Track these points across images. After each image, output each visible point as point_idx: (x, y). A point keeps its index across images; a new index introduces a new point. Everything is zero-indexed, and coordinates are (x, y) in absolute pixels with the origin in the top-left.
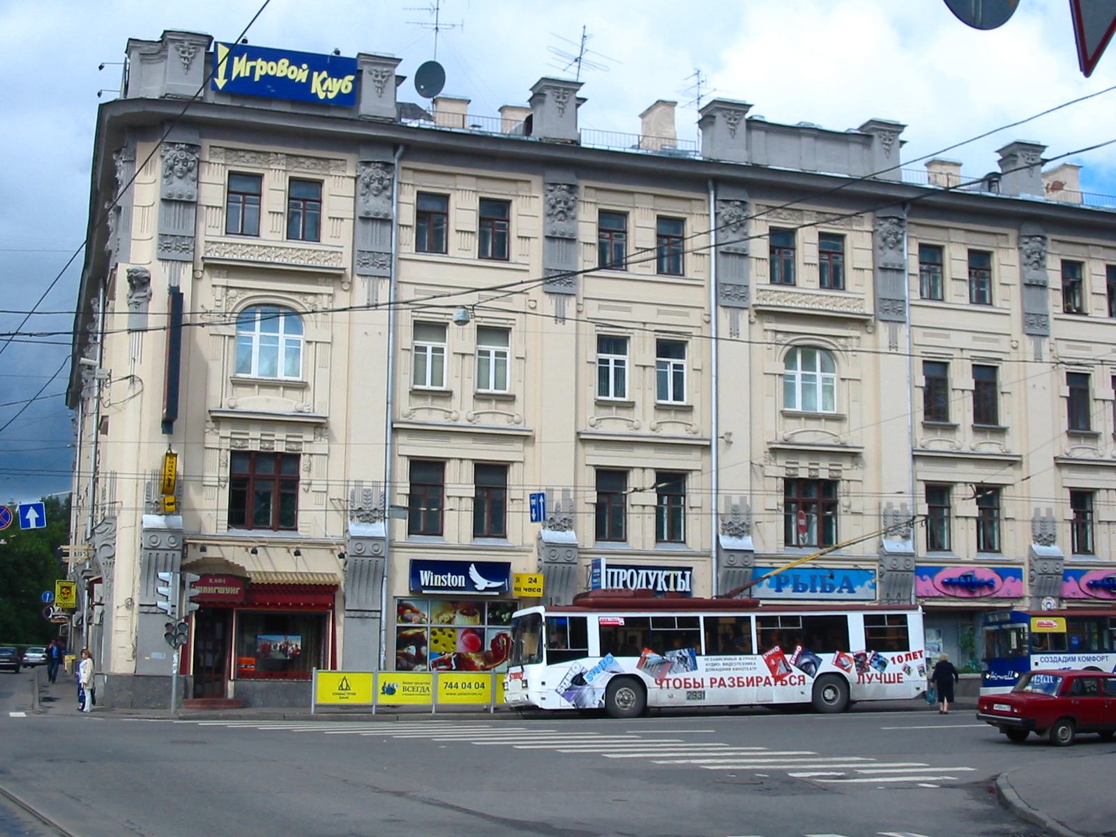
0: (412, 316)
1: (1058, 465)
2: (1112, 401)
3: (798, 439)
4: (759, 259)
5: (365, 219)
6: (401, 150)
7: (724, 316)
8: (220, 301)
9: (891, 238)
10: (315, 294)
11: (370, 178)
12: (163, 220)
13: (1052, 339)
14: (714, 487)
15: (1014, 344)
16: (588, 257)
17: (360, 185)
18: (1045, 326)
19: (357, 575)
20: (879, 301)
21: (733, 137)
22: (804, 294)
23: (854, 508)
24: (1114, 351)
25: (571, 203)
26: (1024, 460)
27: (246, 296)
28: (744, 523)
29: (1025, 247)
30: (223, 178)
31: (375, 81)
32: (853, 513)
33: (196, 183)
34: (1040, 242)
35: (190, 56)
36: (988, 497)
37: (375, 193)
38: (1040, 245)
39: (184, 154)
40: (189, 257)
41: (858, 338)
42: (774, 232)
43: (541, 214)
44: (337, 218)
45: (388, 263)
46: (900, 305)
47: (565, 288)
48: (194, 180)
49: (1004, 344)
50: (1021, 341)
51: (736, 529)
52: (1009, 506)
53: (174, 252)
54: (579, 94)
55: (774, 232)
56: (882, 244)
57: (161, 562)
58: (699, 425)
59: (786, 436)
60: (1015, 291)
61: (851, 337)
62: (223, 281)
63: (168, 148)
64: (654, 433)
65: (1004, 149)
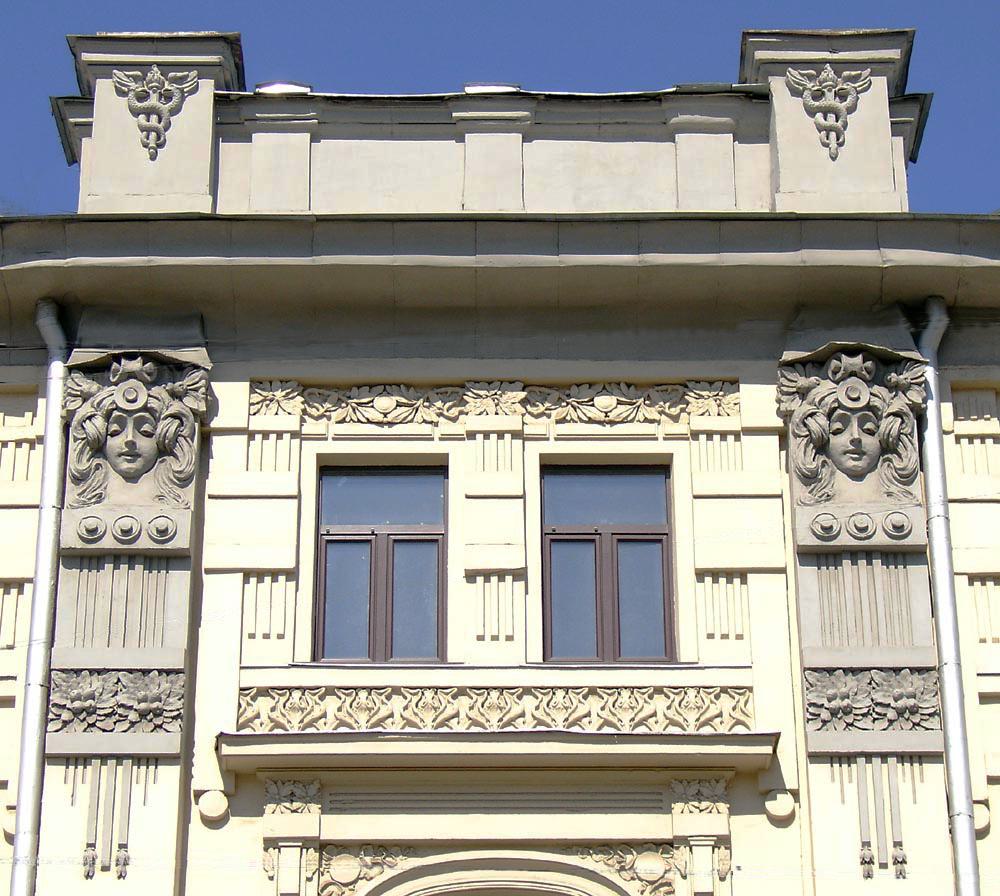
4: (260, 574)
10: (664, 846)
11: (108, 416)
21: (153, 157)
27: (389, 873)
30: (520, 470)
31: (135, 113)
40: (168, 741)
41: (722, 842)
45: (176, 704)
47: (139, 735)
61: (684, 841)
62: (309, 821)
63: (802, 382)
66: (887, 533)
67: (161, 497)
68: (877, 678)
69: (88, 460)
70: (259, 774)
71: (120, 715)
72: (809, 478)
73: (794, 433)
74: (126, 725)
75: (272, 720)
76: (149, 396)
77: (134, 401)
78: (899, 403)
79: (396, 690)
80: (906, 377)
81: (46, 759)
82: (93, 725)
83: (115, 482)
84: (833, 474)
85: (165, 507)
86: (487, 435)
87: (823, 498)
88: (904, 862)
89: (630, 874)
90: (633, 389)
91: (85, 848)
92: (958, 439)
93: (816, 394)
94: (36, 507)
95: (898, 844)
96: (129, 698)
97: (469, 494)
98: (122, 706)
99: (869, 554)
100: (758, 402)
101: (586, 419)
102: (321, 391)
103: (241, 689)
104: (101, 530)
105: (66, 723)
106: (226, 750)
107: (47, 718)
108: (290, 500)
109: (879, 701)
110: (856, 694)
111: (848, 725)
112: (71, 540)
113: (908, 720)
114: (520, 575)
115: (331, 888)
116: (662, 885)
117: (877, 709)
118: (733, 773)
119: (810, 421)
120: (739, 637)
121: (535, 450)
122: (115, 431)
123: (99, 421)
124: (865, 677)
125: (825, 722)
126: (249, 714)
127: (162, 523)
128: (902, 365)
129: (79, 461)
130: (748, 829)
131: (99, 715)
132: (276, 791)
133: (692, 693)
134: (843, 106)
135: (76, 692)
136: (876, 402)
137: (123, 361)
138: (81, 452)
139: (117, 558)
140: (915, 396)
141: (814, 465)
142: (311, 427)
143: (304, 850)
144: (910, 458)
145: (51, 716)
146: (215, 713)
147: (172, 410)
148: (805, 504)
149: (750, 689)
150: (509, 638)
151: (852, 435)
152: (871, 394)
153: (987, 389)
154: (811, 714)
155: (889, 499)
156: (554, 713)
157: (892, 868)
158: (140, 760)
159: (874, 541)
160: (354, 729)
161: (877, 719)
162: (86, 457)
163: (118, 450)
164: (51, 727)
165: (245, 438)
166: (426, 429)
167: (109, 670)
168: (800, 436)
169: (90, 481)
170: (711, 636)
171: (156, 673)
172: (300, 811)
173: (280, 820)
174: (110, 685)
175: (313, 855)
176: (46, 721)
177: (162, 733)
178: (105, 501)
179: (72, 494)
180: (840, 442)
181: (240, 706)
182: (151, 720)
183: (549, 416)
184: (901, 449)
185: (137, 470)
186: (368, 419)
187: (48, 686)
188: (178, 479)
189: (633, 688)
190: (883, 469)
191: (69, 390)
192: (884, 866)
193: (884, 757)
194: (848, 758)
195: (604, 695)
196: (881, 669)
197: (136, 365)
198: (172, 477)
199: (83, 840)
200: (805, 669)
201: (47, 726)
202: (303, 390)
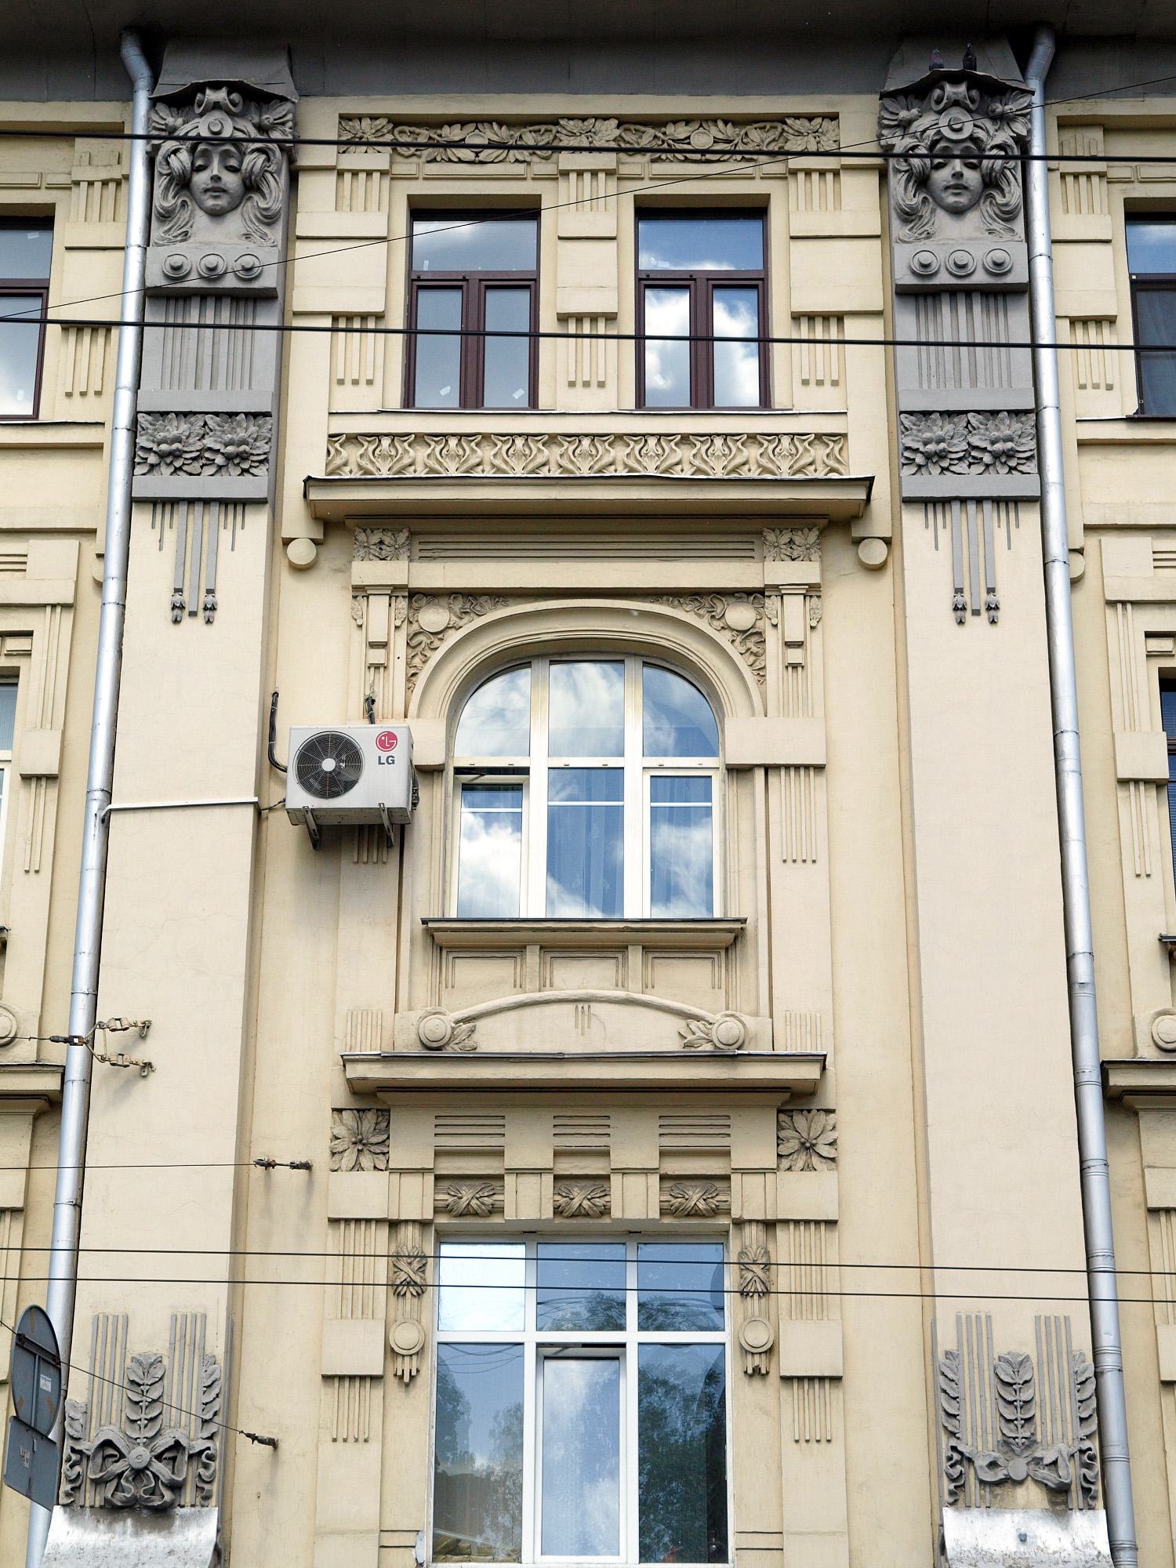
0: (1150, 655)
2: (1158, 784)
3: (493, 1037)
6: (1043, 51)
8: (384, 645)
10: (754, 595)
14: (1105, 1310)
23: (791, 1362)
24: (1161, 560)
28: (177, 1446)
32: (787, 1380)
33: (276, 233)
41: (812, 591)
47: (991, 476)
51: (138, 1473)
59: (438, 1027)
63: (904, 114)
66: (951, 273)
67: (247, 236)
68: (974, 422)
69: (174, 197)
70: (347, 521)
71: (207, 459)
73: (894, 168)
74: (145, 469)
75: (760, 466)
76: (235, 128)
77: (959, 130)
78: (1003, 136)
79: (486, 437)
80: (1011, 107)
81: (133, 501)
82: (180, 469)
83: (201, 220)
84: (933, 211)
85: (252, 245)
86: (580, 173)
87: (923, 236)
88: (997, 608)
89: (720, 624)
91: (953, 594)
92: (1063, 176)
93: (918, 126)
94: (122, 249)
95: (991, 591)
96: (216, 441)
97: (561, 235)
98: (210, 449)
101: (456, 160)
102: (412, 129)
103: (331, 436)
104: (186, 268)
105: (152, 467)
106: (315, 495)
107: (134, 462)
108: (304, 235)
109: (975, 444)
110: (952, 437)
111: (1011, 469)
112: (156, 280)
113: (1005, 463)
115: (420, 638)
116: (752, 634)
117: (973, 453)
118: (826, 521)
119: (173, 159)
120: (835, 383)
122: (200, 166)
123: (184, 156)
124: (963, 418)
125: (920, 467)
126: (338, 461)
127: (248, 261)
128: (1007, 95)
129: (165, 197)
131: (186, 459)
132: (774, 539)
133: (786, 441)
135: (162, 434)
136: (981, 134)
137: (208, 91)
138: (167, 189)
140: (1020, 128)
141: (915, 200)
143: (394, 598)
144: (1013, 194)
145: (137, 460)
147: (998, 141)
148: (905, 242)
149: (845, 436)
150: (601, 385)
151: (953, 169)
152: (235, 128)
153: (680, 121)
154: (907, 458)
155: (990, 236)
156: (513, 462)
157: (984, 614)
158: (1001, 502)
159: (936, 281)
160: (709, 475)
161: (973, 463)
162: (171, 194)
163: (204, 186)
164: (139, 470)
165: (333, 177)
166: (520, 169)
167: (195, 413)
168: (900, 172)
169: (175, 220)
170: (805, 382)
171: (243, 416)
172: (389, 558)
174: (197, 428)
175: (403, 604)
176: (133, 465)
177: (247, 476)
178: (191, 240)
179: (157, 232)
180: (942, 177)
181: (329, 452)
182: (238, 464)
183: (420, 157)
184: (1004, 186)
185: (222, 208)
186: (459, 159)
187: (134, 429)
188: (266, 217)
189: (794, 435)
190: (248, 208)
191: (154, 124)
192: (976, 613)
193: (979, 501)
194: (944, 502)
195: (697, 443)
196: (978, 412)
197: (221, 95)
198: (259, 216)
200: (901, 413)
201: (134, 469)
202: (394, 128)
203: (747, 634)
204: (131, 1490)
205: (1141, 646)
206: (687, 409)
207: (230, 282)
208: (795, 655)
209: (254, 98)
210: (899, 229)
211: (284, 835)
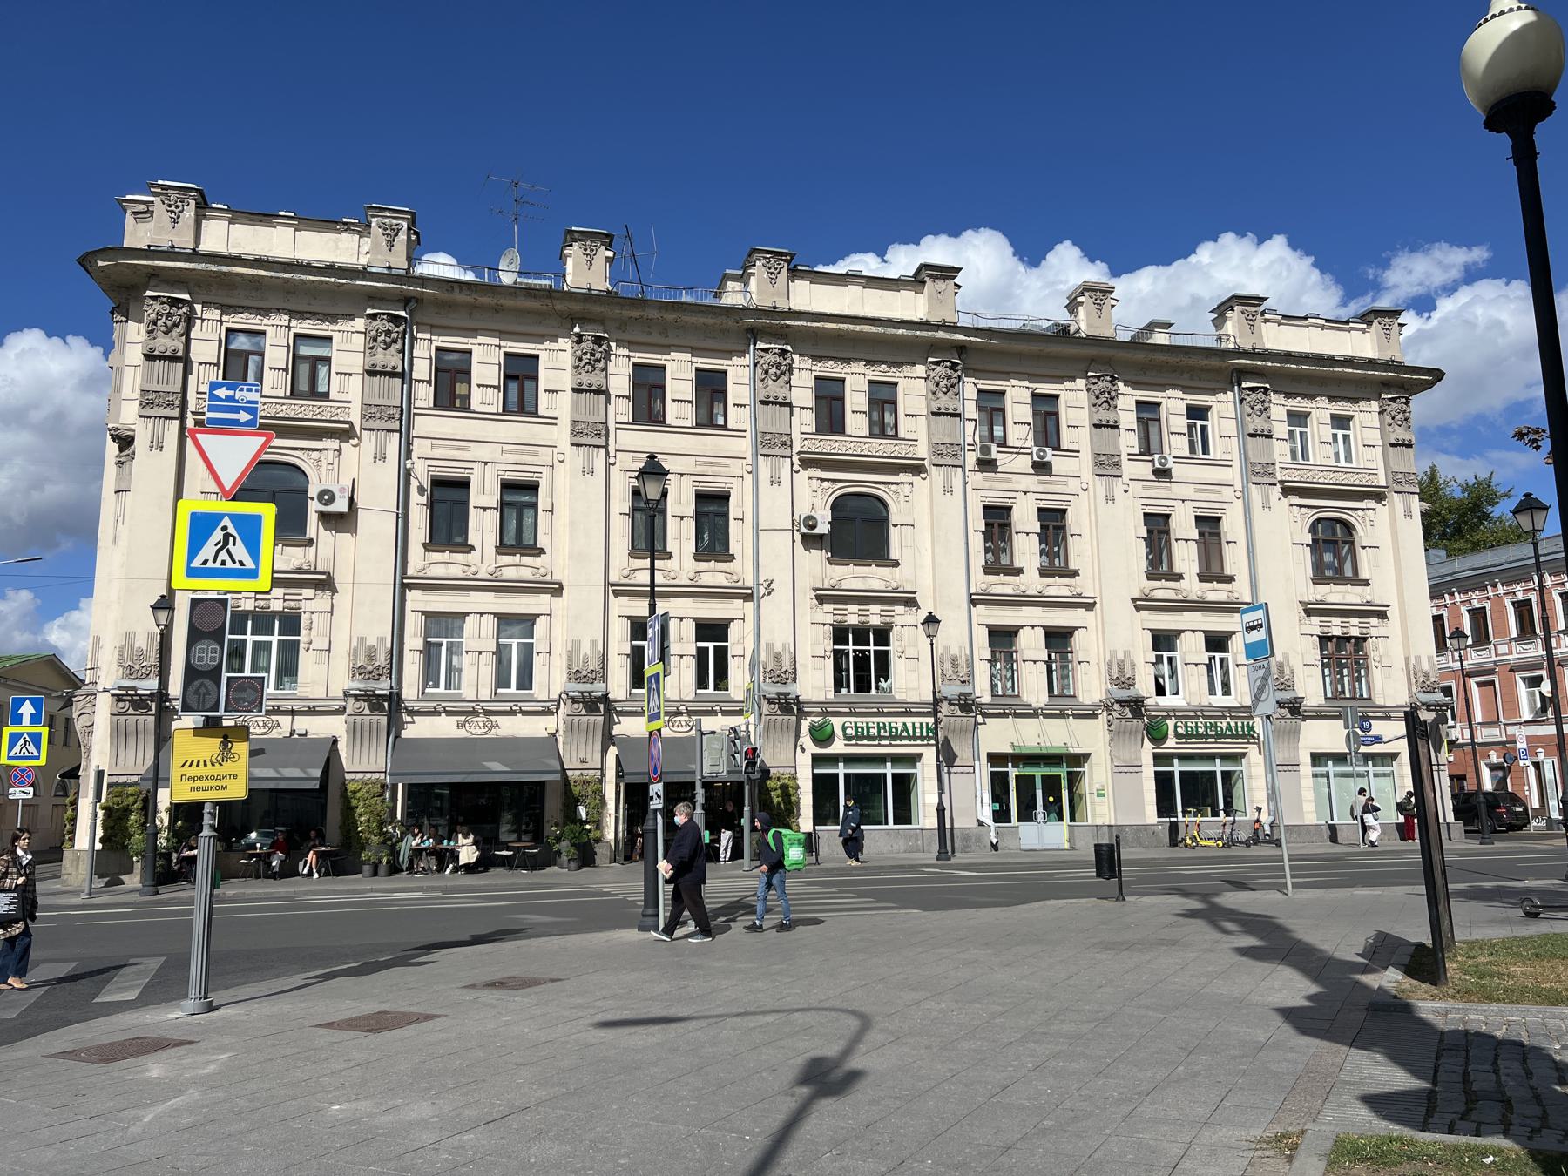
1: (1138, 608)
4: (804, 408)
5: (1097, 426)
7: (1255, 491)
9: (1400, 416)
10: (1363, 510)
12: (147, 378)
13: (1125, 478)
15: (1085, 486)
16: (622, 410)
17: (759, 371)
18: (1118, 465)
19: (772, 731)
20: (936, 448)
21: (390, 250)
22: (1346, 473)
25: (1113, 394)
26: (1097, 600)
29: (1093, 387)
34: (1110, 382)
35: (177, 210)
36: (1058, 639)
37: (944, 390)
38: (1109, 385)
39: (949, 372)
40: (602, 442)
41: (911, 483)
42: (1140, 405)
43: (1086, 404)
44: (346, 374)
45: (398, 416)
46: (1116, 459)
48: (399, 352)
49: (736, 468)
50: (1091, 484)
52: (739, 641)
53: (156, 408)
54: (1400, 321)
55: (1140, 405)
56: (1391, 421)
57: (778, 725)
58: (741, 570)
59: (833, 582)
60: (566, 398)
62: (819, 473)
64: (693, 583)
65: (1219, 306)
72: (934, 393)
90: (892, 364)
93: (154, 307)
99: (947, 414)
100: (920, 370)
112: (367, 368)
114: (811, 409)
121: (1135, 398)
130: (916, 480)
134: (177, 210)
139: (1105, 426)
142: (814, 368)
146: (796, 448)
153: (427, 324)
158: (595, 446)
173: (812, 472)
199: (373, 452)
203: (896, 493)
204: (779, 679)
205: (628, 480)
206: (498, 414)
207: (780, 400)
208: (907, 499)
209: (783, 353)
210: (368, 351)
211: (798, 536)
